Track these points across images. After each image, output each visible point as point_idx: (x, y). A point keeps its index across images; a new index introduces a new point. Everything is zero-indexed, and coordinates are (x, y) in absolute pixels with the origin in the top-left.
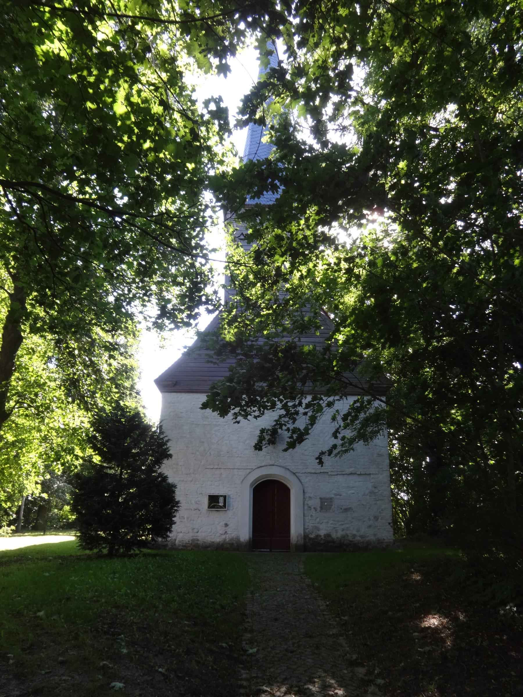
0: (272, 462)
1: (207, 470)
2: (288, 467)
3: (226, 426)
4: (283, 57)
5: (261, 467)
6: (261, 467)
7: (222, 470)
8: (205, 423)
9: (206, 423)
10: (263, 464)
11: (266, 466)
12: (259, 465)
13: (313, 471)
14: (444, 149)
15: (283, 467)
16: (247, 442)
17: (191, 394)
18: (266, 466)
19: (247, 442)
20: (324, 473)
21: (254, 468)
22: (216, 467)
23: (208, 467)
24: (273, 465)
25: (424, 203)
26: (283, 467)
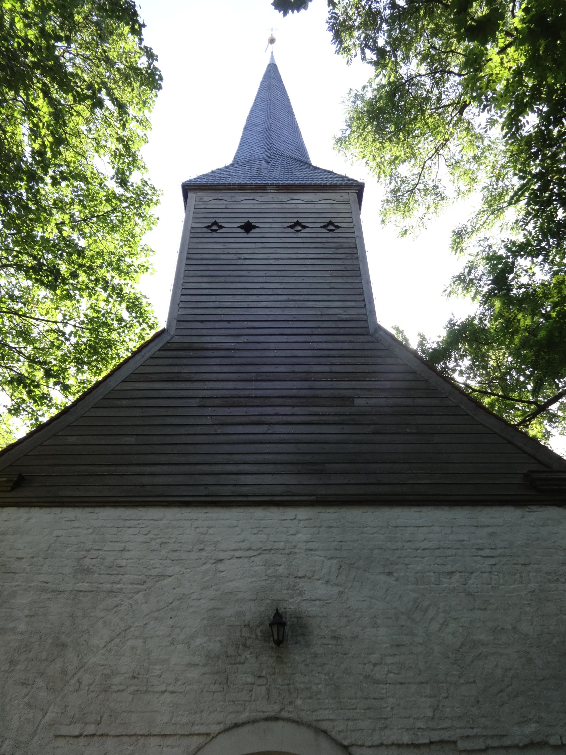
0: (272, 709)
1: (61, 743)
2: (325, 726)
3: (139, 597)
4: (441, 667)
5: (237, 726)
6: (237, 726)
7: (110, 743)
8: (79, 586)
9: (85, 586)
10: (243, 717)
11: (254, 721)
12: (231, 719)
13: (406, 739)
14: (548, 211)
15: (309, 725)
16: (198, 641)
17: (57, 510)
18: (254, 721)
19: (198, 641)
20: (442, 742)
21: (214, 729)
22: (91, 729)
23: (65, 730)
24: (276, 719)
25: (552, 117)
26: (309, 725)
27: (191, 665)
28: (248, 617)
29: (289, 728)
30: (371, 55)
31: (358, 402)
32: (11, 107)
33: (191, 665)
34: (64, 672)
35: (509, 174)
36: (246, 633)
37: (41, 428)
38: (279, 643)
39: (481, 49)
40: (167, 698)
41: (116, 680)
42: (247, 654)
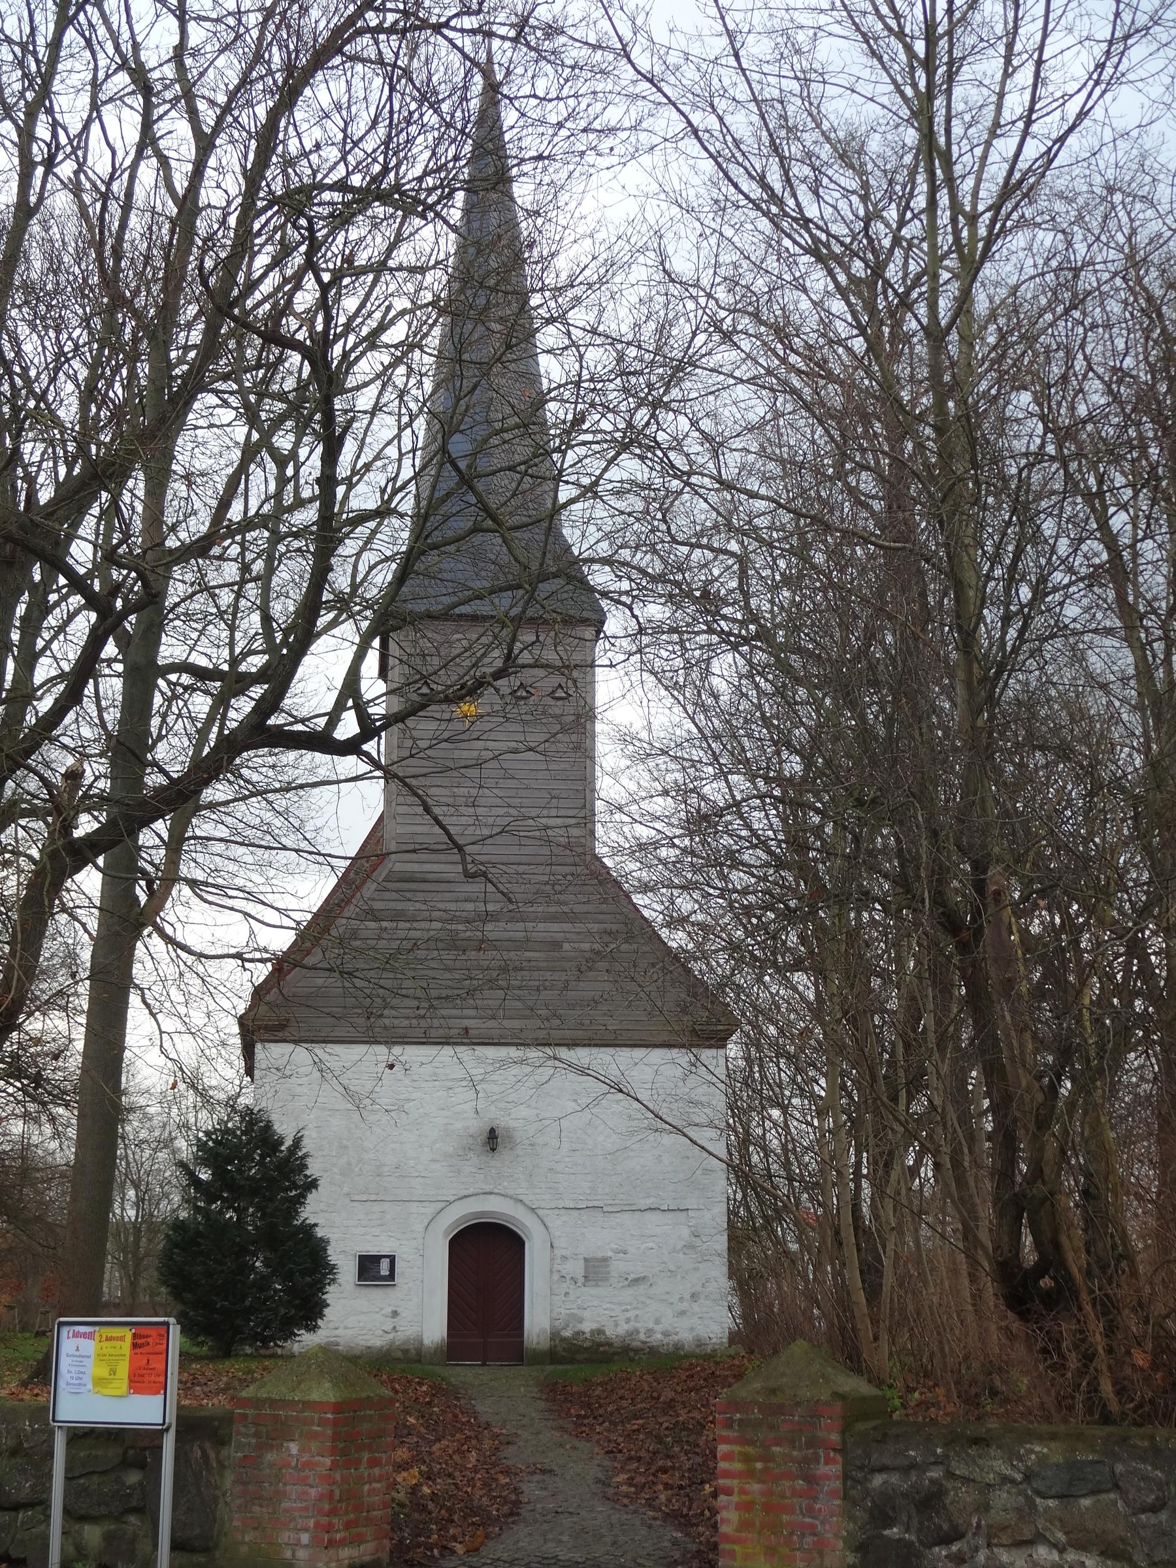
10: (471, 1191)
16: (438, 1146)
21: (452, 1198)
22: (373, 1197)
27: (433, 1160)
28: (472, 1131)
29: (499, 1198)
30: (563, 198)
31: (566, 946)
32: (934, 760)
33: (433, 1160)
34: (349, 1164)
35: (74, 76)
36: (471, 1141)
37: (90, 1014)
38: (493, 1150)
39: (1107, 855)
40: (421, 1180)
41: (386, 1169)
42: (471, 1154)
